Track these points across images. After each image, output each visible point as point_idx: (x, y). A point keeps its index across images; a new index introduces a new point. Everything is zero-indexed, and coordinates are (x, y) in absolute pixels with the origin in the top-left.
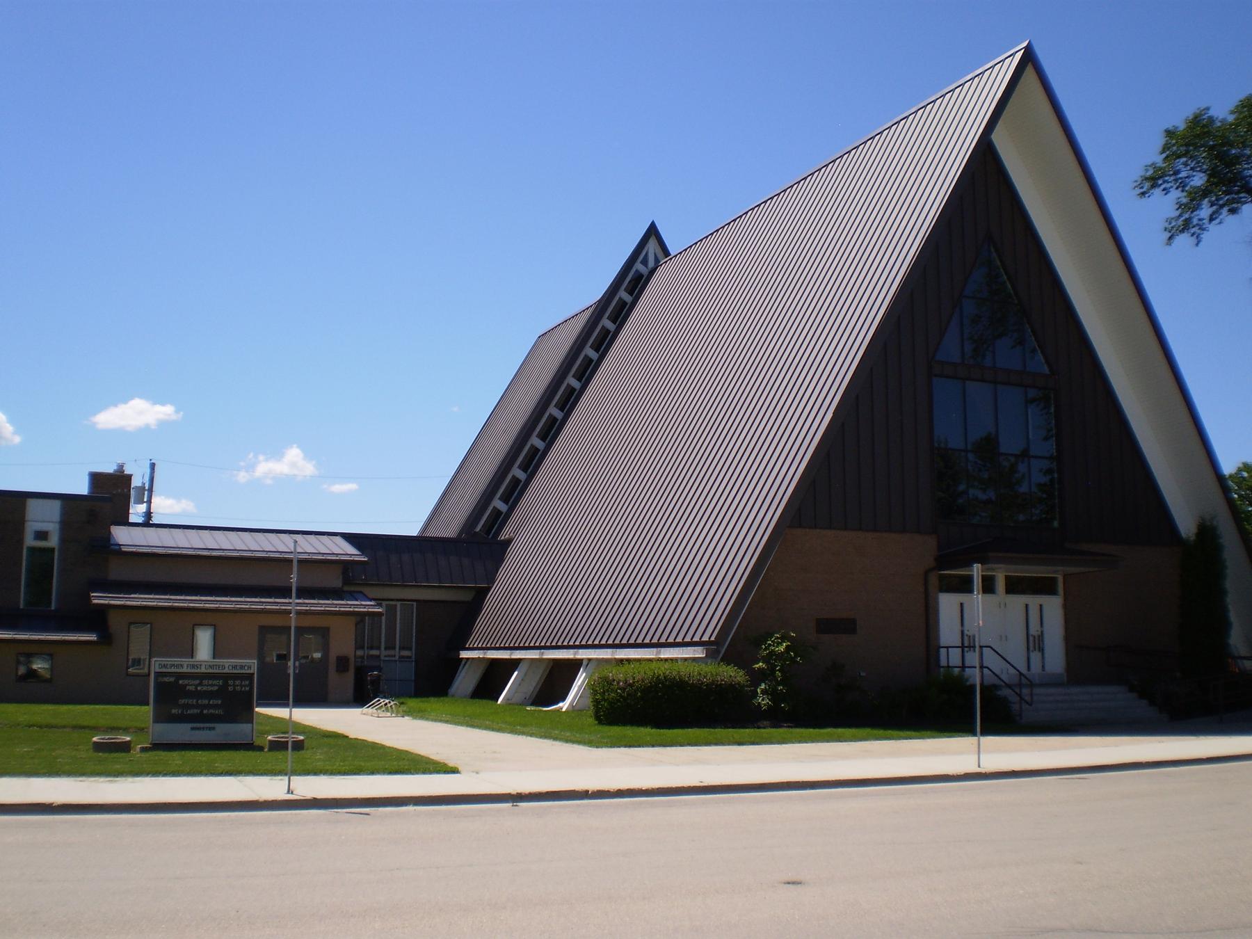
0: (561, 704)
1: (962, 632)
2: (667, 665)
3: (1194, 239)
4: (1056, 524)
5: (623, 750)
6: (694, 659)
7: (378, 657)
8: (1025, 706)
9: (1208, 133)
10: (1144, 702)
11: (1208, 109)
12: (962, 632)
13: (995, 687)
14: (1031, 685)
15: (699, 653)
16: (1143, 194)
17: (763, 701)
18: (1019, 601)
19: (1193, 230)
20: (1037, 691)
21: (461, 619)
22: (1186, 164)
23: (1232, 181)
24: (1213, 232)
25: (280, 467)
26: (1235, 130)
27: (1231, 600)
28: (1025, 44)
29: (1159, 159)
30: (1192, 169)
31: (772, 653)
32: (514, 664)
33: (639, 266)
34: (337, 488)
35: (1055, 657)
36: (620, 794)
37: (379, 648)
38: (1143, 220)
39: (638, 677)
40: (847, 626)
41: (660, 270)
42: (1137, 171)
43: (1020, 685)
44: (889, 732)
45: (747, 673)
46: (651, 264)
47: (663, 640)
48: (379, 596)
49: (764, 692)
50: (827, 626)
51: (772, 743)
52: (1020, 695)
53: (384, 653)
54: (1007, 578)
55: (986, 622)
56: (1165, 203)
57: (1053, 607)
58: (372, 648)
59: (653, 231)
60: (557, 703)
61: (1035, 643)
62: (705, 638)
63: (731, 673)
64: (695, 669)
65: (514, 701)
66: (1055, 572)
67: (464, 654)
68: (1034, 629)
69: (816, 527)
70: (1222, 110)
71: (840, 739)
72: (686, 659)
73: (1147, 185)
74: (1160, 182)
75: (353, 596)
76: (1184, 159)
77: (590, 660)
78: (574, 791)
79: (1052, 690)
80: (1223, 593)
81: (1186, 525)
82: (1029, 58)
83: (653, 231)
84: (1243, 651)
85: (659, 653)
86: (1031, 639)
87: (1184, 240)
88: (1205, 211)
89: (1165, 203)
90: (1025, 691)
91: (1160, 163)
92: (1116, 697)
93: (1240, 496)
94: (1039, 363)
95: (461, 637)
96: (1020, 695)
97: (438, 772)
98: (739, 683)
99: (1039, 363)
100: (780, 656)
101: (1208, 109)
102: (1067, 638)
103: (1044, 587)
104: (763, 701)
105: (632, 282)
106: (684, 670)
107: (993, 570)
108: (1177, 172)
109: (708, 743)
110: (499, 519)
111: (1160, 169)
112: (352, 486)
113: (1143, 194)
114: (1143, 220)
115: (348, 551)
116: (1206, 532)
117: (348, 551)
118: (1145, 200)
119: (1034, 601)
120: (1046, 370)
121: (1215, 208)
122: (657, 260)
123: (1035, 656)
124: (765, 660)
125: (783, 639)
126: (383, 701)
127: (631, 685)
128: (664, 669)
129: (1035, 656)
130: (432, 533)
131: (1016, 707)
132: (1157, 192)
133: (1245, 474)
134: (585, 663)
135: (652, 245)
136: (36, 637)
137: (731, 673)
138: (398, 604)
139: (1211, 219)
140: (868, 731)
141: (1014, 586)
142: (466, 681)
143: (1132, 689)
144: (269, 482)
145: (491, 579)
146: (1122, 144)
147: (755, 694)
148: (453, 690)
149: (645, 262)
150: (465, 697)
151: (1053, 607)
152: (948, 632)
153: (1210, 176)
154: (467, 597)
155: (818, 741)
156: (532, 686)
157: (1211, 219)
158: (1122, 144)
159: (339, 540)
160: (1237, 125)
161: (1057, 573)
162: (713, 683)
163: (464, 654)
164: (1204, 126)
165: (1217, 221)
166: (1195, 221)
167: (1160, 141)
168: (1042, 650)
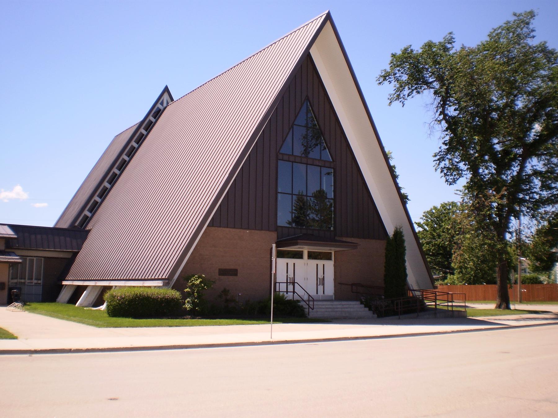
0: (101, 307)
1: (287, 276)
2: (142, 289)
3: (401, 104)
4: (332, 229)
5: (112, 329)
6: (159, 287)
7: (24, 283)
8: (310, 310)
9: (410, 57)
10: (367, 309)
11: (411, 46)
12: (287, 276)
13: (298, 301)
14: (314, 300)
15: (160, 283)
16: (380, 83)
17: (188, 306)
18: (314, 262)
19: (400, 100)
20: (315, 303)
21: (64, 267)
22: (399, 71)
23: (419, 79)
24: (409, 101)
25: (11, 195)
26: (421, 56)
27: (407, 264)
28: (327, 12)
29: (388, 70)
30: (402, 73)
31: (193, 284)
32: (85, 287)
33: (159, 105)
34: (38, 205)
35: (330, 288)
36: (88, 351)
37: (25, 279)
38: (378, 95)
39: (127, 294)
40: (234, 272)
41: (168, 107)
42: (378, 73)
43: (309, 300)
44: (244, 321)
45: (182, 294)
46: (165, 105)
47: (146, 278)
48: (22, 254)
49: (188, 302)
50: (224, 272)
51: (186, 326)
52: (308, 305)
53: (27, 281)
54: (309, 252)
55: (305, 274)
56: (390, 87)
57: (329, 265)
58: (21, 279)
59: (166, 90)
60: (99, 306)
61: (321, 282)
62: (164, 277)
63: (176, 294)
64: (157, 291)
65: (83, 305)
66: (331, 250)
67: (64, 283)
68: (320, 275)
69: (220, 227)
70: (417, 48)
71: (220, 324)
72: (155, 287)
73: (382, 79)
74: (387, 78)
75: (9, 254)
76: (398, 68)
77: (116, 286)
78: (64, 349)
79: (329, 303)
80: (404, 261)
81: (391, 231)
82: (328, 17)
83: (166, 90)
84: (415, 287)
85: (143, 283)
86: (319, 279)
87: (397, 104)
88: (406, 91)
89: (390, 87)
90: (311, 303)
91: (388, 70)
92: (355, 307)
93: (431, 220)
94: (327, 156)
95: (64, 276)
96: (308, 305)
97: (6, 338)
98: (176, 298)
99: (327, 156)
100: (197, 286)
101: (411, 46)
102: (335, 280)
103: (327, 257)
104: (188, 306)
105: (156, 112)
106: (149, 292)
107: (302, 248)
108: (396, 74)
109: (155, 326)
110: (87, 220)
111: (388, 72)
112: (45, 204)
113: (380, 83)
114: (378, 95)
115: (9, 232)
116: (398, 234)
117: (9, 232)
118: (381, 86)
119: (320, 263)
120: (331, 160)
121: (410, 90)
122: (168, 103)
123: (320, 288)
124: (190, 288)
125: (199, 277)
126: (16, 304)
127: (123, 298)
128: (138, 291)
129: (320, 288)
130: (59, 226)
131: (307, 310)
132: (386, 83)
133: (434, 211)
134: (114, 288)
135: (166, 96)
136: (34, 270)
137: (176, 294)
138: (35, 258)
139: (408, 95)
140: (235, 321)
141: (312, 256)
142: (65, 295)
143: (362, 303)
144: (6, 201)
145: (80, 247)
146: (371, 59)
147: (184, 304)
148: (58, 300)
149: (162, 104)
150: (64, 303)
151: (329, 265)
152: (281, 277)
153: (410, 76)
154: (69, 256)
155: (208, 325)
156: (93, 297)
157: (408, 95)
158: (371, 59)
159: (6, 227)
160: (423, 54)
161: (332, 251)
162: (163, 298)
163: (64, 283)
164: (408, 53)
165: (411, 96)
166: (402, 96)
167: (390, 59)
168: (323, 284)
